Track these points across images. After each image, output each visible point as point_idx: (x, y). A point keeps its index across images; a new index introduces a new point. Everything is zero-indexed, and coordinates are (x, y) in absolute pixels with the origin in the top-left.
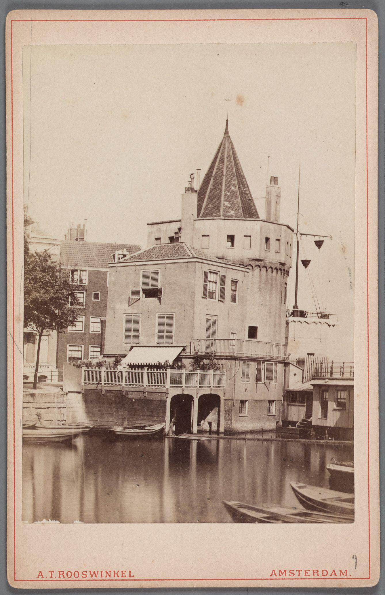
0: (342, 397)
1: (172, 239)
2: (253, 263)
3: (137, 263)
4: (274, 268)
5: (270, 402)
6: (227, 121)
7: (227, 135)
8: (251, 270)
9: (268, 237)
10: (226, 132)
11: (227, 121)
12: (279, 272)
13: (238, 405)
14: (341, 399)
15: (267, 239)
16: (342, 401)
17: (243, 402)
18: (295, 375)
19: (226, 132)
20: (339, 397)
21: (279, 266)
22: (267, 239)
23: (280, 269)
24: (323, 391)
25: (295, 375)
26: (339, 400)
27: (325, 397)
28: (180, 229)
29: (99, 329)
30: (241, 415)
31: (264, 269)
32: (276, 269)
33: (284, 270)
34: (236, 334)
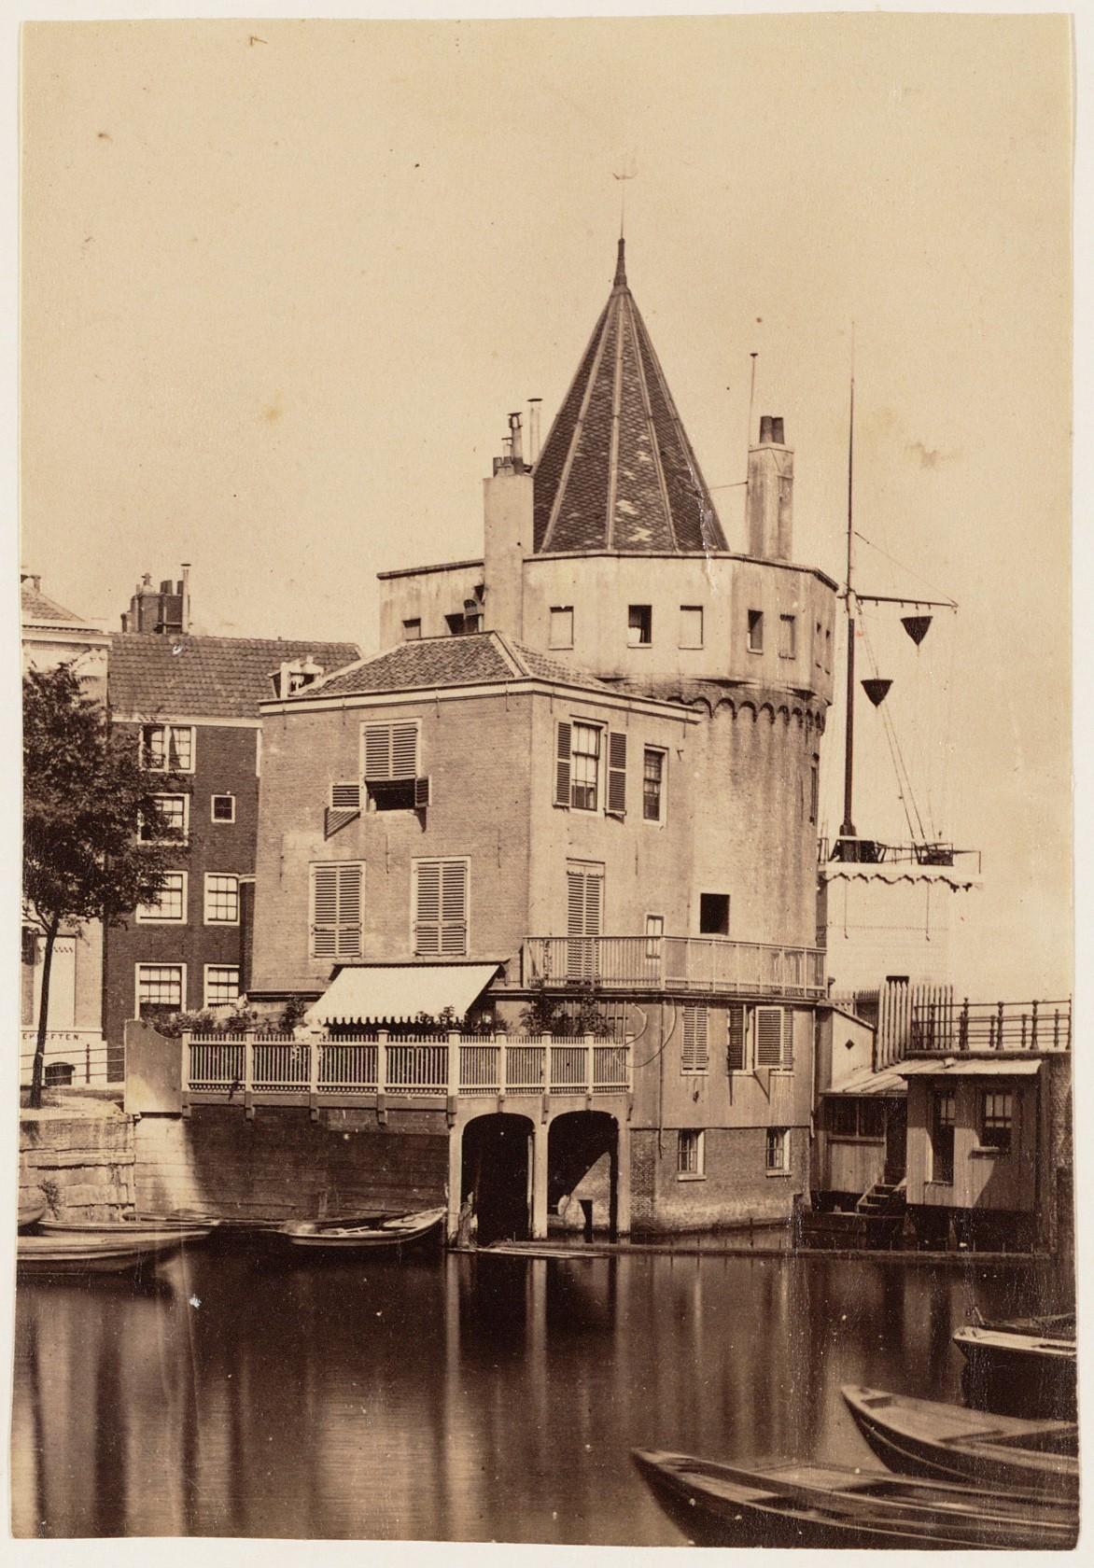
0: (999, 1113)
1: (456, 623)
2: (713, 694)
3: (349, 702)
4: (776, 706)
5: (774, 1133)
6: (622, 242)
7: (621, 288)
8: (706, 716)
9: (757, 608)
10: (620, 280)
11: (622, 242)
13: (671, 1142)
14: (995, 1119)
15: (755, 617)
16: (1000, 1125)
17: (688, 1135)
18: (849, 1045)
19: (620, 280)
20: (989, 1113)
21: (791, 702)
22: (755, 617)
23: (797, 711)
24: (984, 1094)
25: (849, 1045)
26: (989, 1124)
27: (943, 1114)
29: (232, 913)
30: (681, 1177)
31: (745, 713)
32: (783, 709)
33: (809, 713)
34: (661, 918)
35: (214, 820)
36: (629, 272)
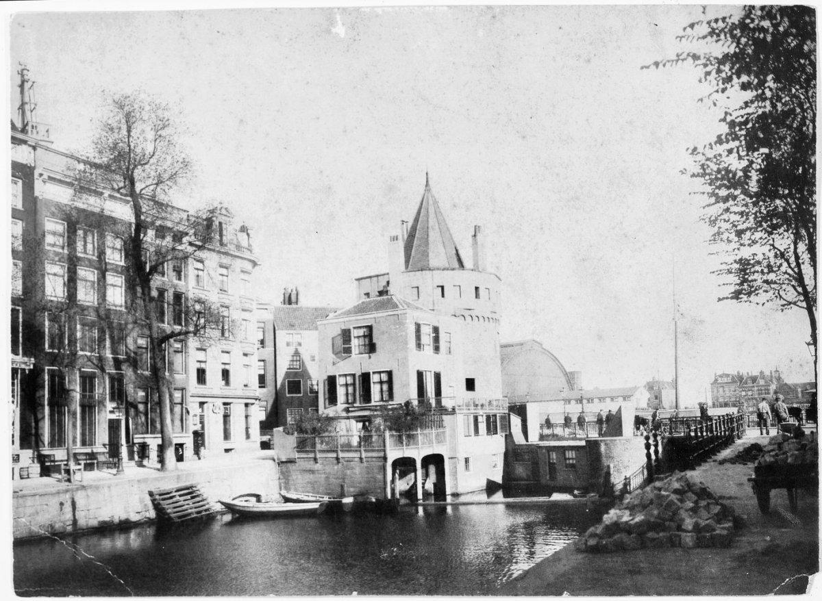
0: (571, 457)
1: (381, 293)
2: (467, 313)
12: (737, 287)
14: (569, 459)
16: (571, 461)
19: (427, 185)
22: (477, 288)
26: (568, 462)
28: (388, 283)
35: (288, 395)
36: (430, 183)
